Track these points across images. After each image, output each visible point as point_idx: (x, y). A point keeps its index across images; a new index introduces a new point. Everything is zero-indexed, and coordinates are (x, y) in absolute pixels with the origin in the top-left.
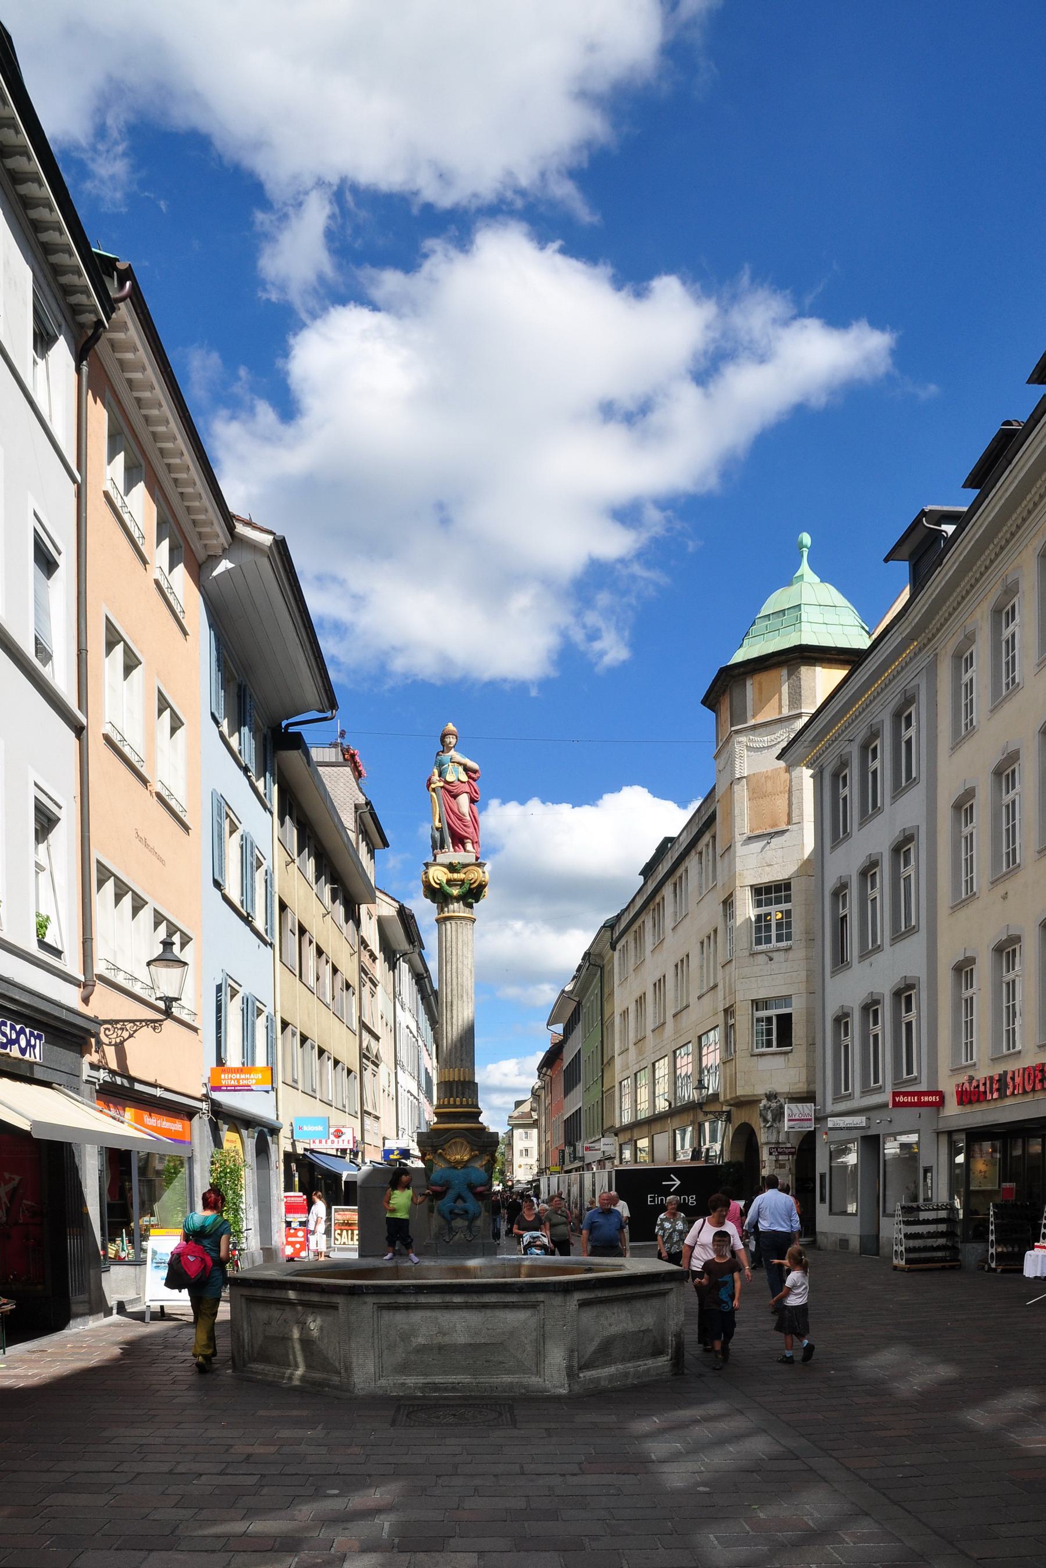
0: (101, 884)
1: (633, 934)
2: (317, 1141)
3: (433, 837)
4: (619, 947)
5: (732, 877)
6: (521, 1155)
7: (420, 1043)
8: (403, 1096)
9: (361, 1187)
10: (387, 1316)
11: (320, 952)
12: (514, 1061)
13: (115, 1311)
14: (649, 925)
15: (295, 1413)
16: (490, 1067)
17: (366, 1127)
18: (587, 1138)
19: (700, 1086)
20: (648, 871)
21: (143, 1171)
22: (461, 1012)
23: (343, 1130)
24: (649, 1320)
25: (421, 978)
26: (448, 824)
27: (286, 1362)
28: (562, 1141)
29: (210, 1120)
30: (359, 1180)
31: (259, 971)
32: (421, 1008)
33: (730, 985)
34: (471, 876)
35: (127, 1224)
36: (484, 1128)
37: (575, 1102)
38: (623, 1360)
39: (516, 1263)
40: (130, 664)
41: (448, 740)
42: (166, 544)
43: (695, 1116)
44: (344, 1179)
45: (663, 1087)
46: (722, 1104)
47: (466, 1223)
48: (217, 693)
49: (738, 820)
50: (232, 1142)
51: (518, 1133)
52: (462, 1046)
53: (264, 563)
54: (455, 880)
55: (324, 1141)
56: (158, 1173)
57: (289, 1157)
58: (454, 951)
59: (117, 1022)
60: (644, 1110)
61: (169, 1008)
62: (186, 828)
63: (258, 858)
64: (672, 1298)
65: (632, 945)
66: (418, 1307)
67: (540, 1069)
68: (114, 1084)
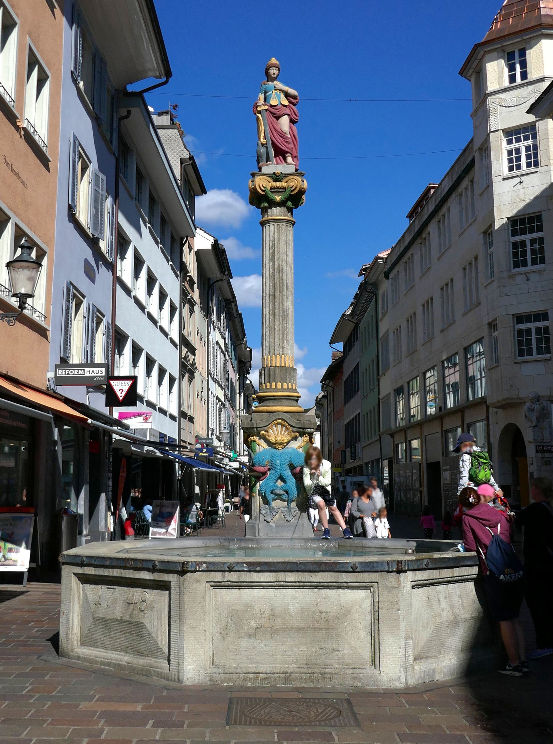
4: (391, 275)
14: (417, 258)
26: (272, 140)
28: (343, 443)
34: (291, 184)
65: (403, 274)
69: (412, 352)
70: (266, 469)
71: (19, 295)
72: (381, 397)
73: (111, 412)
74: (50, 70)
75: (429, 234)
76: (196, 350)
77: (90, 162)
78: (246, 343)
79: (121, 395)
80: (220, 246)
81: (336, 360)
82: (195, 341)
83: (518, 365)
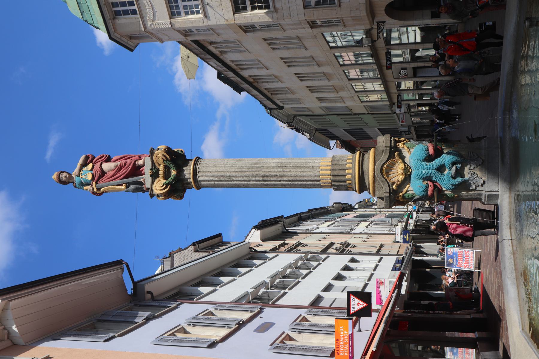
1: (274, 96)
3: (135, 190)
4: (281, 104)
7: (339, 220)
14: (267, 86)
19: (359, 43)
26: (123, 178)
32: (317, 219)
34: (160, 160)
41: (64, 179)
54: (164, 173)
58: (220, 174)
69: (336, 89)
72: (366, 112)
73: (376, 311)
75: (250, 76)
77: (208, 310)
78: (331, 207)
79: (363, 305)
82: (326, 243)
83: (341, 4)
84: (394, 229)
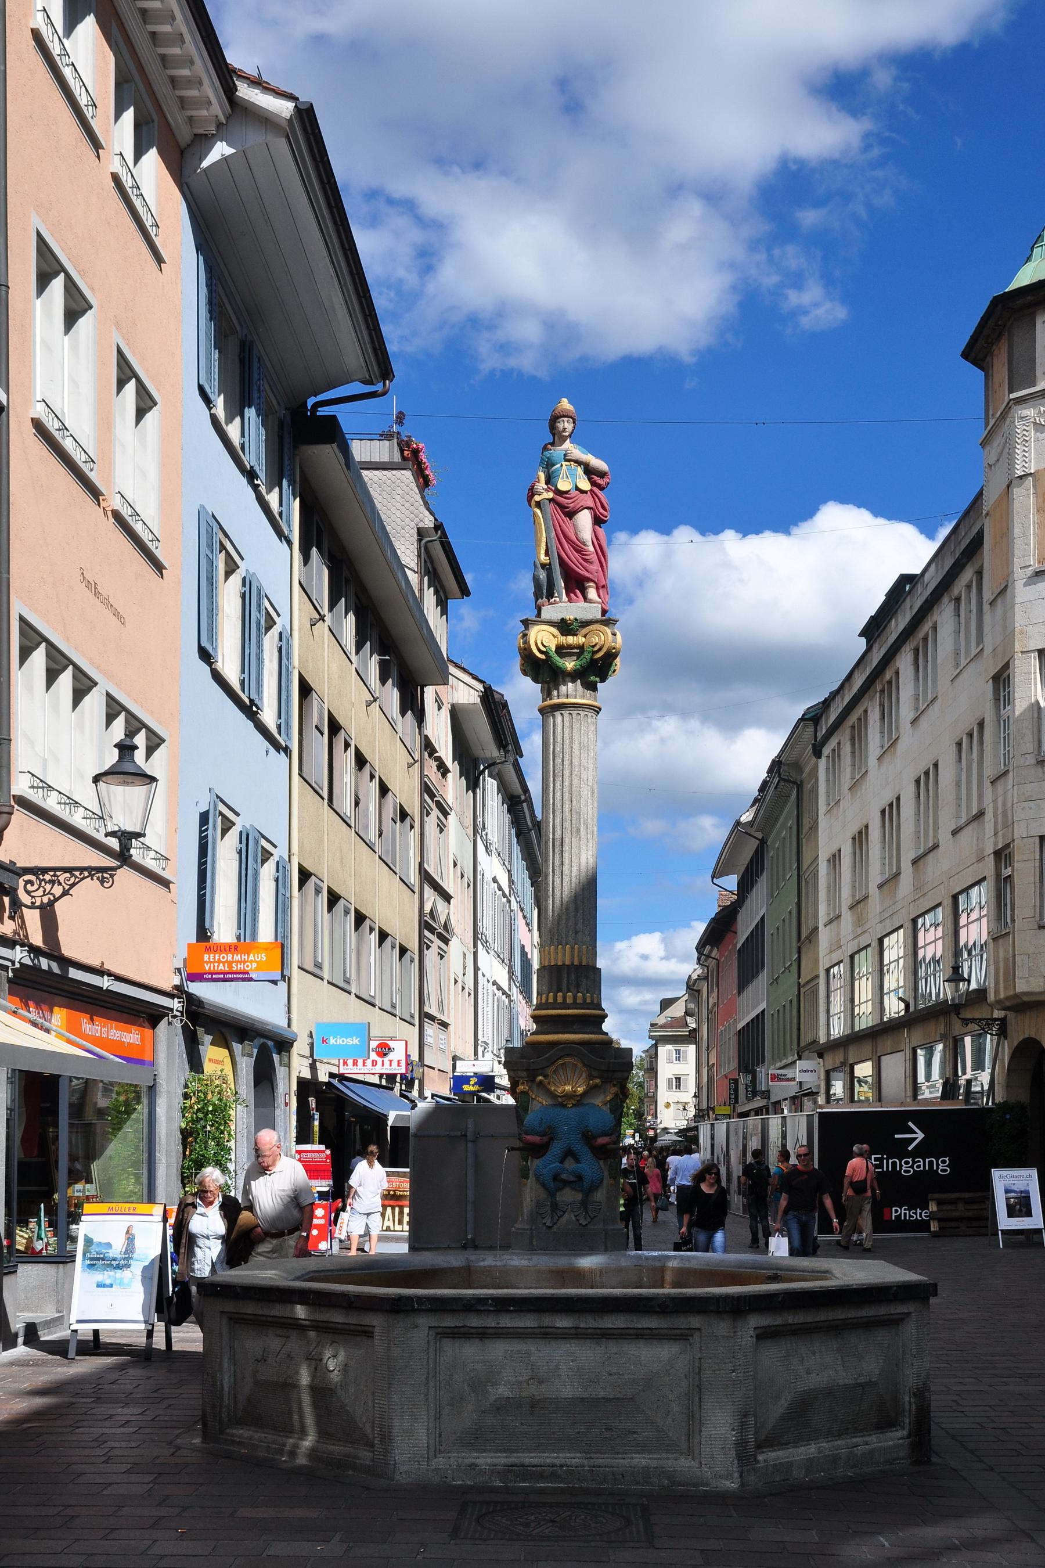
0: (25, 653)
1: (848, 732)
2: (350, 1062)
3: (536, 580)
4: (826, 751)
5: (1008, 636)
6: (670, 1087)
7: (514, 905)
8: (486, 990)
9: (415, 1135)
10: (451, 1349)
11: (361, 761)
12: (657, 935)
13: (20, 1340)
14: (874, 716)
15: (298, 1513)
16: (621, 945)
17: (428, 1040)
18: (774, 1061)
19: (956, 976)
20: (873, 630)
21: (78, 1109)
22: (577, 856)
23: (391, 1044)
24: (871, 1366)
25: (516, 803)
26: (560, 557)
27: (286, 1426)
28: (734, 1065)
29: (185, 1028)
30: (412, 1125)
31: (266, 792)
32: (516, 849)
33: (1005, 812)
34: (595, 640)
35: (47, 1196)
36: (610, 1042)
37: (756, 1001)
38: (830, 1434)
39: (658, 1264)
40: (75, 310)
41: (560, 426)
42: (129, 116)
43: (948, 1026)
44: (390, 1123)
45: (896, 979)
46: (992, 1006)
47: (579, 1196)
48: (209, 359)
49: (1018, 543)
50: (217, 1062)
51: (665, 1051)
52: (577, 909)
53: (281, 146)
54: (570, 647)
55: (360, 1062)
56: (101, 1113)
57: (305, 1088)
58: (567, 758)
59: (45, 870)
60: (866, 1016)
61: (125, 848)
62: (158, 567)
63: (268, 613)
64: (910, 1328)
65: (847, 748)
66: (500, 1334)
67: (700, 948)
68: (36, 969)
70: (545, 1139)
71: (119, 834)
74: (158, 390)
75: (897, 673)
76: (452, 897)
80: (496, 696)
81: (726, 907)
82: (449, 885)
84: (489, 1056)
